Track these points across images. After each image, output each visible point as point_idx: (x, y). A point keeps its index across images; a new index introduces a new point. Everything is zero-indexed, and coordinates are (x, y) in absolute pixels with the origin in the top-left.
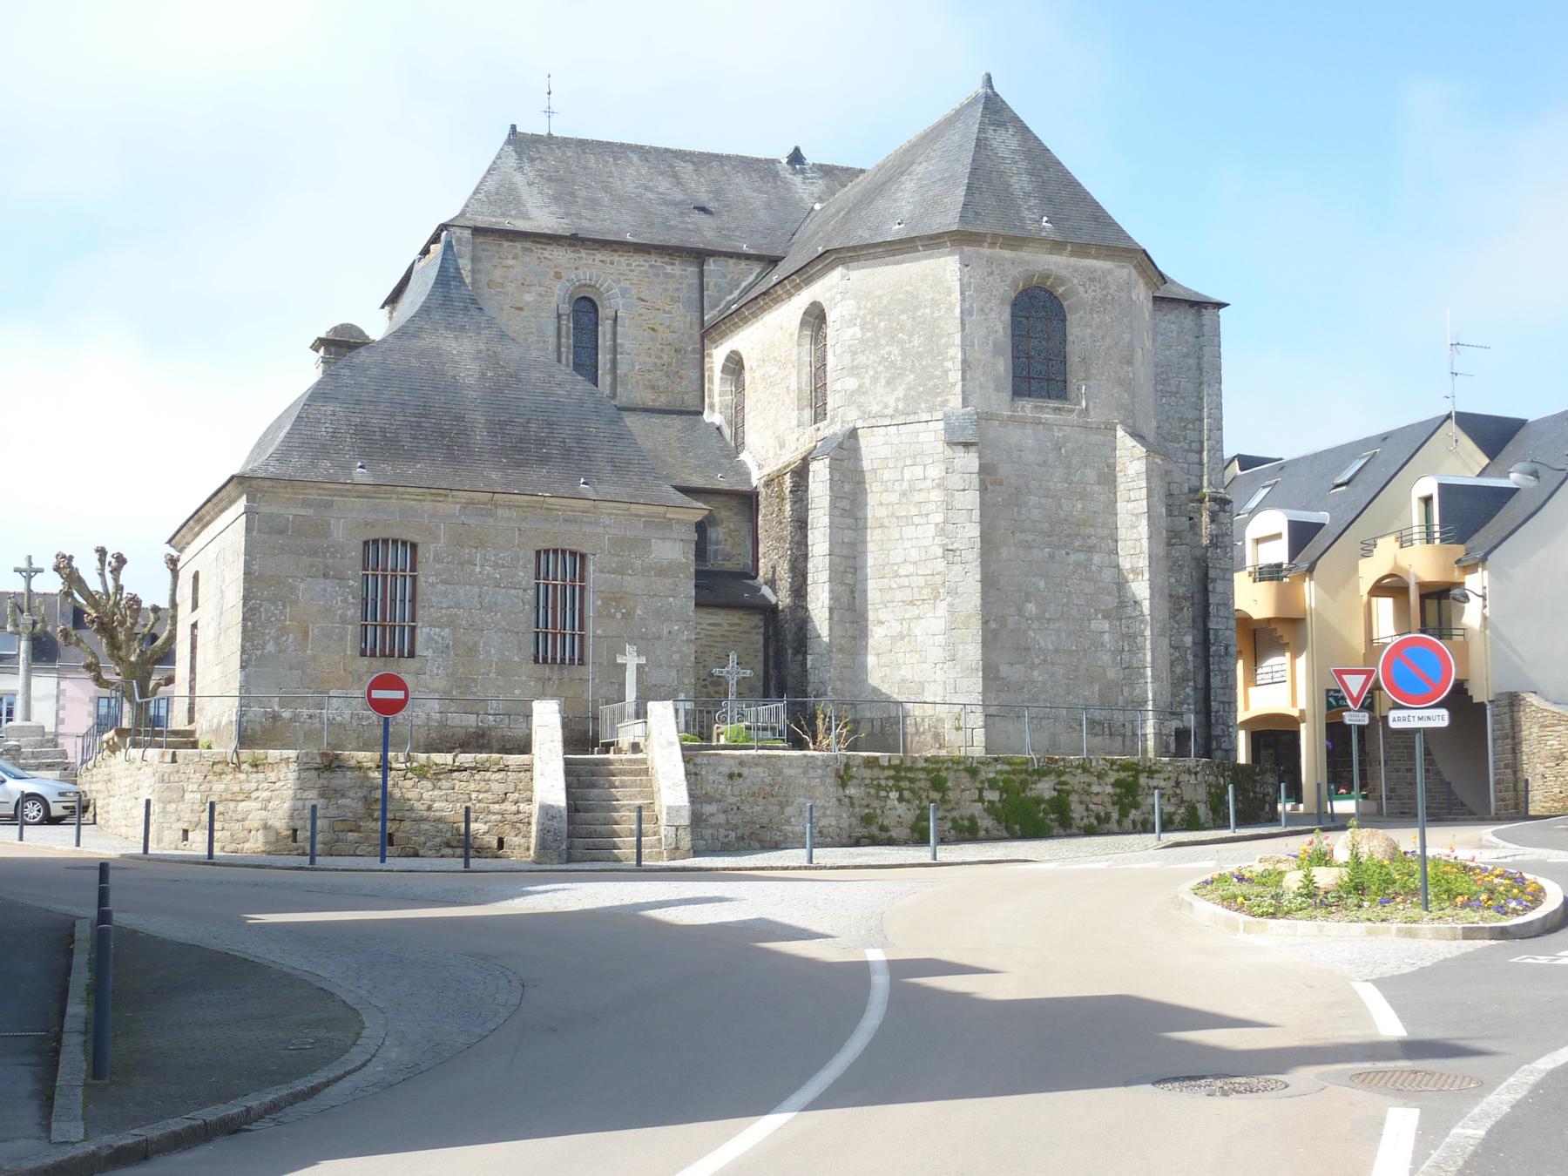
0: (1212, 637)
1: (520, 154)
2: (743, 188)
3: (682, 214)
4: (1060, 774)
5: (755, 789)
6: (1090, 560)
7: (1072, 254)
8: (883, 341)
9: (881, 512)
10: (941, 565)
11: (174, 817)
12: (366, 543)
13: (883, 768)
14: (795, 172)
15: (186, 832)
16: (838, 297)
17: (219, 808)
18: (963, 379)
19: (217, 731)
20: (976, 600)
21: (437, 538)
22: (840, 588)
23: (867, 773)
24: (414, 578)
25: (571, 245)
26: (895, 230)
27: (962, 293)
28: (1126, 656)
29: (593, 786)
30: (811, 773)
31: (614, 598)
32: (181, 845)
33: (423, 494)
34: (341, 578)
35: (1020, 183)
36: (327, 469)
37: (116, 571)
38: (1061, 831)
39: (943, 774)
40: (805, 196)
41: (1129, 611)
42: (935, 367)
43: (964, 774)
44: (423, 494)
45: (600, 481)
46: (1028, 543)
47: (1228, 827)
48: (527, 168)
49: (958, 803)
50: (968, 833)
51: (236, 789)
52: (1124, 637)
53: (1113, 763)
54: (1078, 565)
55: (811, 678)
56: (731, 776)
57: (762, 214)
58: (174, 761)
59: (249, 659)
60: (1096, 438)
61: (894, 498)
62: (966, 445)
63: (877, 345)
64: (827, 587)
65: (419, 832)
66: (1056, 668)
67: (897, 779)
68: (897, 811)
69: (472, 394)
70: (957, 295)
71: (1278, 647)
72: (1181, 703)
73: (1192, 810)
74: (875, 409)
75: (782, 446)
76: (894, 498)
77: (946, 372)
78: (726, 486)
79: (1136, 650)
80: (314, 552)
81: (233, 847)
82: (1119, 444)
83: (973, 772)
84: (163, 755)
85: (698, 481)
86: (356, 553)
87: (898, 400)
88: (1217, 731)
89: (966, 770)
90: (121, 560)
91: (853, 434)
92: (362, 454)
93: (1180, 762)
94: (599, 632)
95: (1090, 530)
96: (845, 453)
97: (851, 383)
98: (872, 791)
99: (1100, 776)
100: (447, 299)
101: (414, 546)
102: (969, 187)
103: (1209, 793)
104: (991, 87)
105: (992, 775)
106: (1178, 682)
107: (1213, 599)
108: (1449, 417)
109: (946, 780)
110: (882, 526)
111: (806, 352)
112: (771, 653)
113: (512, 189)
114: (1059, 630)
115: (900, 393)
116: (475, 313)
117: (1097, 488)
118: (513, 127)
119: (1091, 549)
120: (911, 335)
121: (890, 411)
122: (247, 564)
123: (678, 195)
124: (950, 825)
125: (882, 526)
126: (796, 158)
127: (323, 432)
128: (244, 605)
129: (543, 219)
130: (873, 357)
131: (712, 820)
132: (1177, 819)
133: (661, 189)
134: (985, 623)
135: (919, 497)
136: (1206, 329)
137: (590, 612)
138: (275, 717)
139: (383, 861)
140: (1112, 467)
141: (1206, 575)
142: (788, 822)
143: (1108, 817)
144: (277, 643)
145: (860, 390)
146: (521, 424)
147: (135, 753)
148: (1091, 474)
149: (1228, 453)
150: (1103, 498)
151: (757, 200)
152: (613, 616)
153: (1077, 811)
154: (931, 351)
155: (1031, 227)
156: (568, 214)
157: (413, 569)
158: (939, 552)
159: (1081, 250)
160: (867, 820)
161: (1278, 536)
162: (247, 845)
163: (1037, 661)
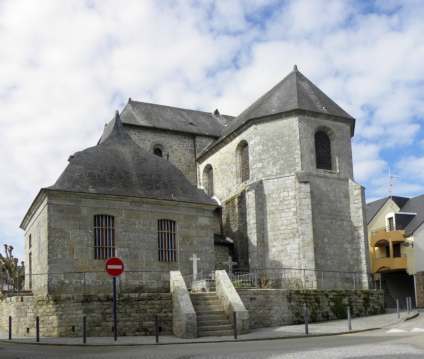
1: (133, 106)
2: (202, 119)
5: (260, 304)
6: (343, 224)
7: (333, 120)
8: (271, 150)
9: (273, 209)
11: (23, 323)
12: (95, 216)
13: (301, 294)
15: (28, 329)
16: (254, 136)
17: (41, 319)
18: (301, 161)
19: (40, 290)
20: (311, 236)
21: (121, 215)
22: (260, 235)
23: (296, 296)
24: (113, 230)
26: (274, 111)
27: (299, 131)
28: (355, 256)
30: (279, 297)
31: (186, 238)
32: (26, 334)
33: (116, 198)
35: (313, 97)
36: (79, 188)
37: (10, 251)
39: (318, 296)
41: (356, 241)
43: (324, 296)
44: (116, 198)
45: (179, 196)
48: (136, 110)
51: (48, 311)
52: (354, 250)
54: (339, 225)
56: (251, 299)
57: (210, 126)
58: (22, 300)
59: (51, 261)
61: (277, 203)
62: (305, 183)
63: (269, 151)
64: (256, 234)
65: (125, 326)
69: (131, 165)
70: (298, 132)
74: (269, 173)
75: (230, 191)
76: (277, 203)
77: (295, 159)
79: (359, 254)
81: (48, 334)
82: (350, 185)
84: (17, 299)
86: (91, 220)
89: (325, 295)
90: (12, 248)
91: (261, 182)
92: (92, 184)
94: (181, 250)
95: (342, 214)
96: (259, 188)
97: (260, 165)
98: (298, 303)
101: (113, 218)
102: (298, 96)
104: (297, 70)
105: (332, 297)
108: (390, 197)
110: (273, 213)
111: (239, 159)
113: (132, 115)
114: (335, 247)
116: (129, 139)
117: (344, 199)
119: (343, 220)
120: (281, 147)
121: (274, 174)
122: (49, 224)
124: (321, 315)
125: (273, 213)
126: (217, 112)
127: (76, 175)
128: (48, 240)
129: (142, 122)
130: (267, 156)
135: (286, 203)
137: (178, 242)
138: (63, 283)
139: (116, 339)
140: (348, 192)
142: (272, 316)
145: (263, 167)
146: (149, 175)
147: (8, 299)
148: (342, 195)
151: (208, 123)
152: (186, 244)
157: (113, 226)
160: (298, 315)
162: (54, 334)
163: (329, 258)
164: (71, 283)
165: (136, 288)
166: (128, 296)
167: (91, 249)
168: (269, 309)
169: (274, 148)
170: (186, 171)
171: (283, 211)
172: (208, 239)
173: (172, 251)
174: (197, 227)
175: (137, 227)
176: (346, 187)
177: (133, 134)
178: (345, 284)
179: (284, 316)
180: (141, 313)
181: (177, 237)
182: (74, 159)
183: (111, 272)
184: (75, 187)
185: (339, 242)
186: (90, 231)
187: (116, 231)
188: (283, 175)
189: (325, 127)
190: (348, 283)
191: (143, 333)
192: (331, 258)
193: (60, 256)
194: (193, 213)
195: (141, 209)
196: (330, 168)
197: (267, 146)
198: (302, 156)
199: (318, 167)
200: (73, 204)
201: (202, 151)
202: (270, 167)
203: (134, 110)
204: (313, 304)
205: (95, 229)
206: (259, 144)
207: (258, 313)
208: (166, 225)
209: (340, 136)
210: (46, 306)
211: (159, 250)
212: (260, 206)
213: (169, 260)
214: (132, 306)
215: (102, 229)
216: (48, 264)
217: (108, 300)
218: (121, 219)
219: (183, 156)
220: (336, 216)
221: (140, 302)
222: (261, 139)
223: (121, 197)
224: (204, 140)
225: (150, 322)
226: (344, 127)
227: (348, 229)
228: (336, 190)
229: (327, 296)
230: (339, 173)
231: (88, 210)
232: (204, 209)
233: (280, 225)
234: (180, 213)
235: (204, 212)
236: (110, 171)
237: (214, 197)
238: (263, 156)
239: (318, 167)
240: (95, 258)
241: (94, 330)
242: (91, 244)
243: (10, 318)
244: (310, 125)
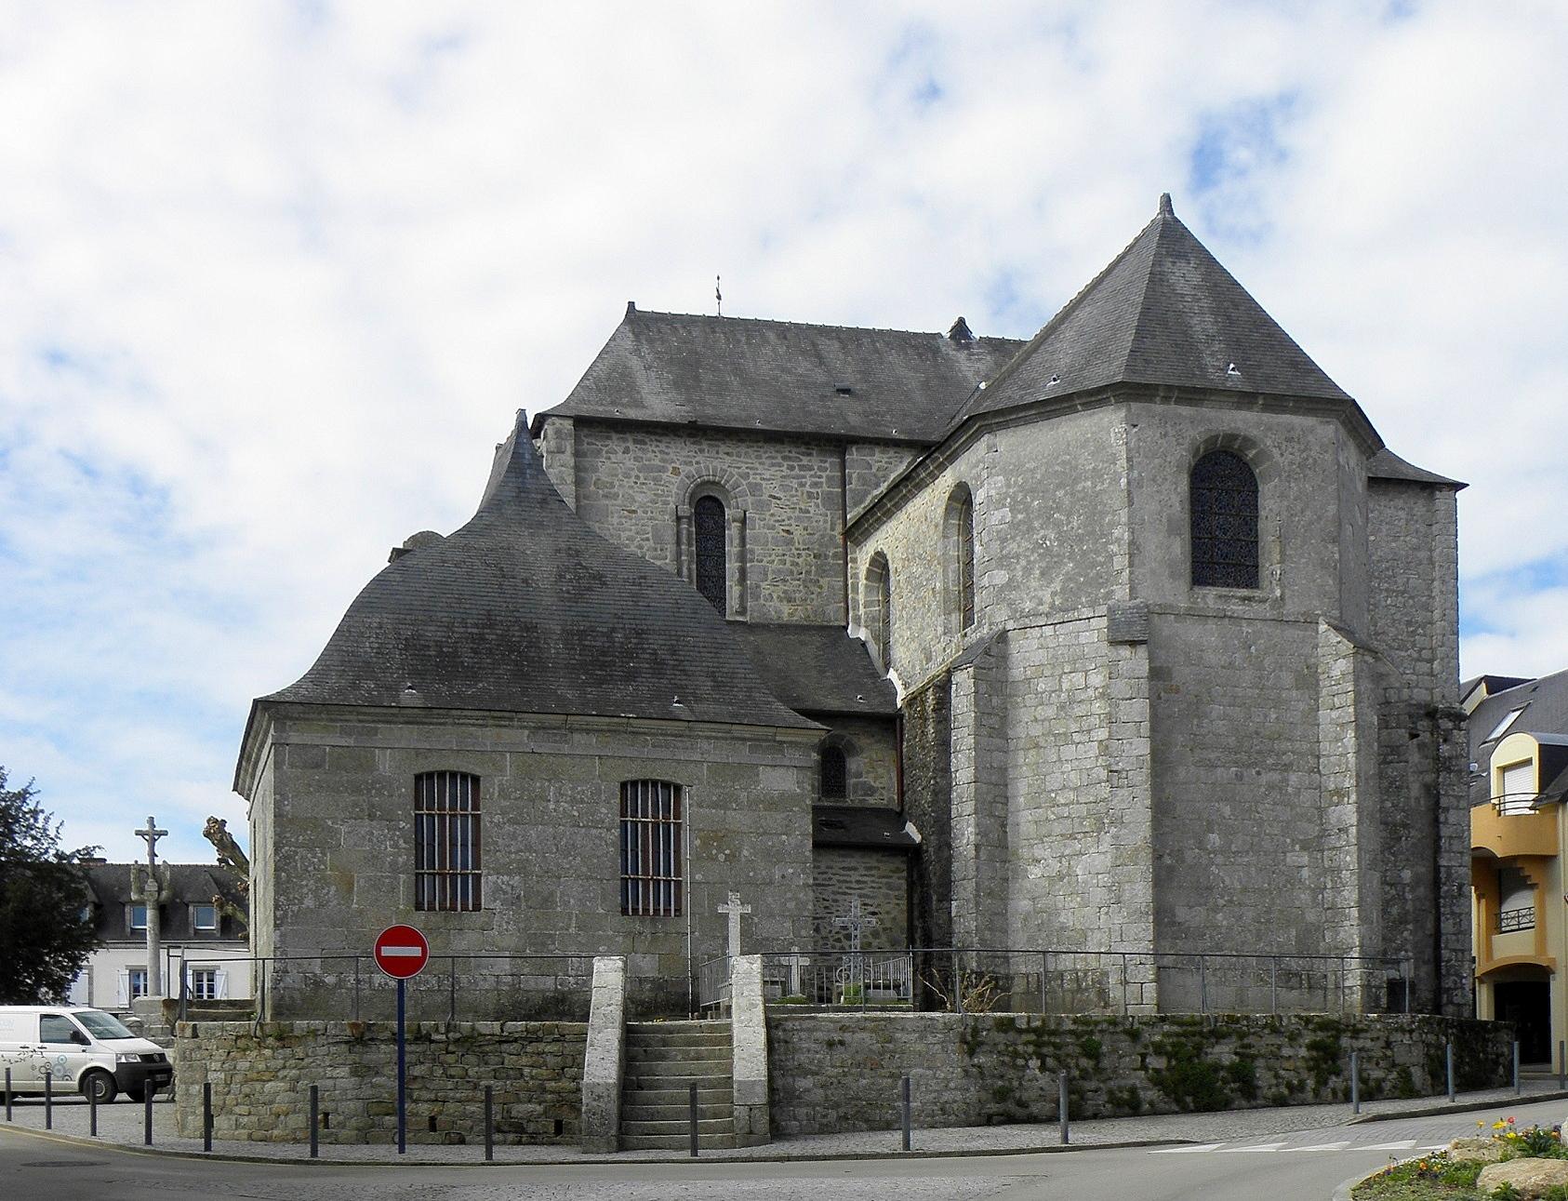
0: (1443, 875)
1: (637, 335)
3: (823, 397)
4: (1242, 1036)
5: (859, 1058)
6: (1286, 780)
7: (1267, 408)
8: (1036, 524)
9: (1036, 730)
10: (1105, 791)
12: (418, 778)
13: (1020, 1031)
14: (960, 347)
18: (1131, 565)
21: (502, 770)
23: (1000, 1038)
24: (477, 818)
25: (690, 435)
26: (1050, 388)
28: (1328, 894)
29: (663, 1057)
30: (930, 1039)
31: (715, 838)
33: (484, 718)
34: (389, 818)
35: (1203, 324)
38: (1244, 1103)
40: (970, 375)
41: (1333, 841)
42: (1097, 553)
43: (1123, 1037)
45: (698, 699)
46: (1193, 751)
47: (1446, 1093)
48: (645, 349)
49: (1114, 1071)
50: (1130, 1107)
51: (261, 1066)
52: (1325, 871)
53: (1308, 1021)
54: (1271, 787)
55: (956, 928)
56: (831, 1044)
58: (195, 1035)
60: (1293, 633)
61: (1051, 712)
62: (1133, 643)
63: (1031, 529)
64: (972, 820)
65: (464, 1116)
66: (1244, 909)
67: (1038, 1045)
68: (1037, 1081)
71: (1523, 884)
72: (1398, 950)
73: (1405, 1075)
74: (1028, 606)
75: (929, 659)
76: (1051, 712)
77: (1111, 557)
78: (866, 709)
80: (357, 790)
82: (1321, 641)
83: (1134, 1035)
85: (833, 703)
86: (407, 790)
87: (1054, 594)
88: (1448, 983)
89: (1126, 1032)
91: (1003, 637)
92: (414, 673)
93: (1391, 1020)
97: (1001, 577)
99: (1293, 1038)
100: (522, 490)
101: (476, 780)
103: (1427, 1055)
104: (1171, 212)
105: (1157, 1038)
106: (1393, 925)
107: (1444, 831)
109: (1100, 1044)
110: (1037, 746)
112: (916, 901)
114: (1248, 865)
115: (1057, 586)
116: (556, 506)
117: (1294, 693)
118: (631, 304)
119: (1287, 767)
120: (1069, 515)
123: (820, 376)
125: (1037, 746)
126: (960, 329)
127: (367, 647)
128: (276, 851)
129: (660, 404)
131: (807, 1097)
132: (1387, 1086)
133: (800, 371)
134: (1158, 858)
136: (1440, 515)
137: (687, 854)
138: (318, 984)
139: (402, 1151)
141: (1437, 803)
143: (1302, 1087)
144: (316, 897)
145: (1011, 585)
148: (1287, 678)
149: (1465, 677)
150: (1301, 706)
151: (913, 380)
152: (715, 859)
153: (1263, 1077)
154: (1093, 533)
155: (1214, 375)
156: (689, 401)
157: (475, 807)
158: (1104, 774)
159: (1276, 403)
160: (1001, 1095)
161: (1528, 762)
163: (1221, 902)
164: (340, 984)
166: (473, 1028)
168: (892, 1076)
169: (1048, 520)
170: (808, 572)
171: (1066, 738)
172: (793, 841)
173: (668, 883)
175: (552, 806)
176: (1307, 650)
177: (620, 450)
178: (1283, 993)
179: (946, 1096)
180: (508, 1077)
181: (686, 836)
182: (409, 561)
183: (392, 965)
184: (359, 688)
185: (1266, 844)
186: (402, 824)
187: (485, 822)
189: (1232, 437)
191: (511, 1137)
192: (1231, 901)
193: (309, 902)
194: (743, 754)
195: (566, 749)
197: (1027, 509)
198: (1134, 549)
200: (351, 742)
201: (869, 498)
202: (1034, 584)
203: (637, 351)
204: (1072, 1063)
205: (418, 818)
206: (1000, 504)
207: (854, 1086)
208: (649, 801)
209: (1291, 463)
210: (255, 1053)
212: (994, 721)
213: (656, 911)
214: (483, 1058)
215: (442, 817)
216: (276, 925)
217: (416, 1039)
218: (501, 784)
219: (798, 518)
220: (1258, 752)
221: (505, 1046)
222: (1009, 486)
223: (499, 711)
224: (878, 458)
225: (530, 1107)
226: (1312, 430)
227: (1307, 798)
228: (1266, 662)
229: (1134, 1035)
230: (1282, 597)
231: (395, 756)
232: (782, 743)
233: (1056, 786)
234: (697, 757)
235: (781, 751)
236: (476, 626)
237: (892, 675)
238: (1012, 547)
241: (381, 1125)
242: (405, 864)
243: (207, 1087)
244: (1172, 433)
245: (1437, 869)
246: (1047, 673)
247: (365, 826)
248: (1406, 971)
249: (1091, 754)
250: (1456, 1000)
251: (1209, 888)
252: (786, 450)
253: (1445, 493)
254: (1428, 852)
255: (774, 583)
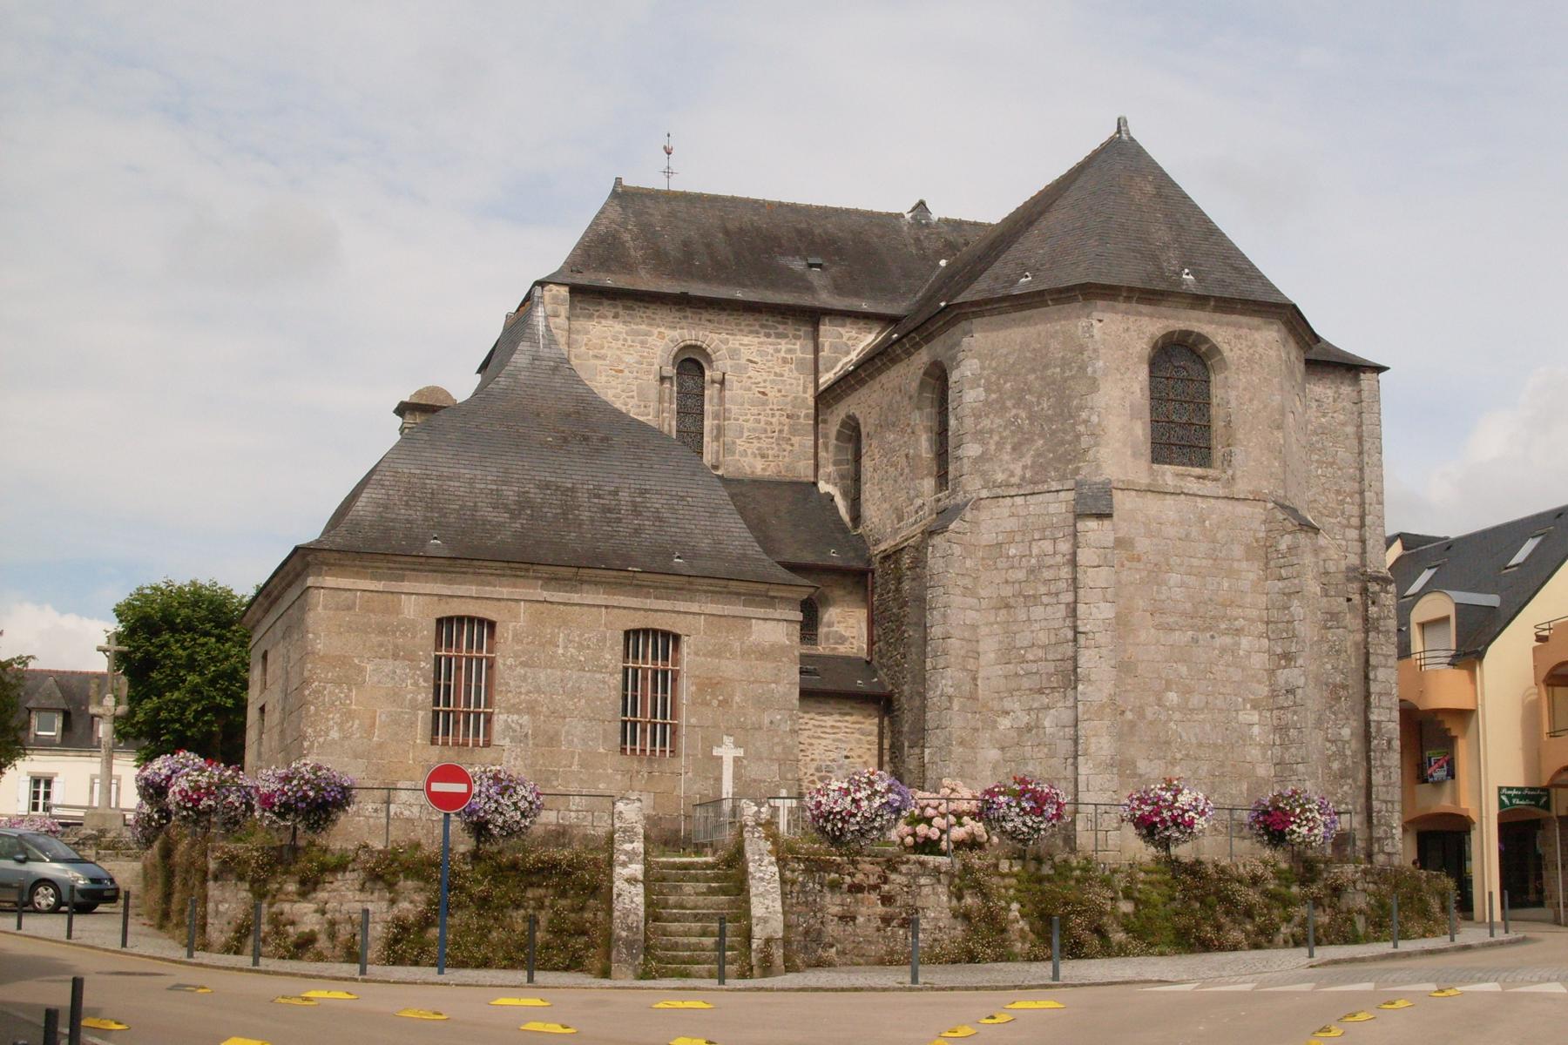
0: (1373, 730)
6: (1238, 644)
8: (1009, 404)
12: (440, 621)
21: (516, 617)
31: (709, 685)
33: (503, 568)
34: (411, 657)
35: (1161, 234)
42: (1065, 432)
54: (1223, 650)
61: (1021, 575)
63: (1004, 408)
72: (1338, 803)
74: (1000, 477)
75: (900, 519)
76: (1021, 575)
78: (840, 563)
80: (383, 631)
86: (428, 631)
87: (1025, 467)
94: (693, 721)
95: (1237, 612)
107: (1374, 688)
110: (1007, 606)
112: (886, 745)
115: (1028, 460)
117: (1244, 565)
118: (618, 181)
120: (1040, 396)
125: (1007, 606)
130: (998, 421)
144: (341, 729)
145: (982, 458)
157: (490, 650)
159: (1227, 305)
161: (1446, 619)
163: (1179, 756)
165: (548, 832)
167: (423, 717)
170: (781, 431)
171: (1035, 599)
174: (745, 654)
175: (560, 651)
187: (499, 663)
188: (1040, 488)
190: (1244, 838)
196: (1205, 461)
199: (1156, 458)
202: (1006, 457)
209: (1240, 358)
211: (624, 723)
219: (773, 381)
220: (1213, 618)
222: (983, 368)
232: (774, 597)
233: (1026, 643)
239: (1156, 458)
240: (433, 742)
245: (1367, 723)
246: (1018, 538)
247: (389, 665)
248: (1344, 823)
249: (1059, 615)
250: (1388, 849)
251: (1168, 743)
252: (764, 318)
253: (1368, 375)
254: (1360, 708)
255: (749, 441)
